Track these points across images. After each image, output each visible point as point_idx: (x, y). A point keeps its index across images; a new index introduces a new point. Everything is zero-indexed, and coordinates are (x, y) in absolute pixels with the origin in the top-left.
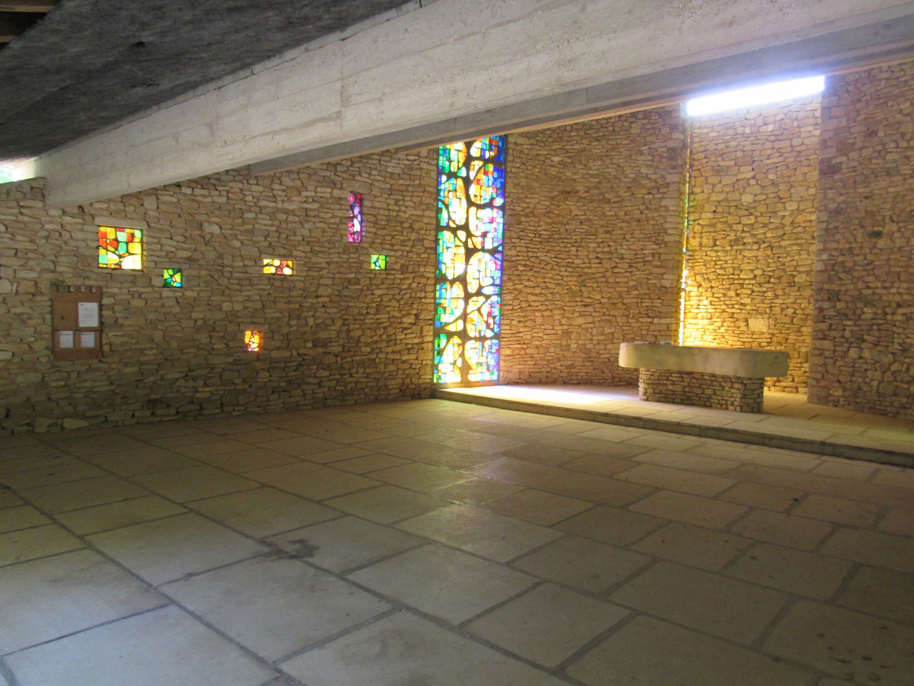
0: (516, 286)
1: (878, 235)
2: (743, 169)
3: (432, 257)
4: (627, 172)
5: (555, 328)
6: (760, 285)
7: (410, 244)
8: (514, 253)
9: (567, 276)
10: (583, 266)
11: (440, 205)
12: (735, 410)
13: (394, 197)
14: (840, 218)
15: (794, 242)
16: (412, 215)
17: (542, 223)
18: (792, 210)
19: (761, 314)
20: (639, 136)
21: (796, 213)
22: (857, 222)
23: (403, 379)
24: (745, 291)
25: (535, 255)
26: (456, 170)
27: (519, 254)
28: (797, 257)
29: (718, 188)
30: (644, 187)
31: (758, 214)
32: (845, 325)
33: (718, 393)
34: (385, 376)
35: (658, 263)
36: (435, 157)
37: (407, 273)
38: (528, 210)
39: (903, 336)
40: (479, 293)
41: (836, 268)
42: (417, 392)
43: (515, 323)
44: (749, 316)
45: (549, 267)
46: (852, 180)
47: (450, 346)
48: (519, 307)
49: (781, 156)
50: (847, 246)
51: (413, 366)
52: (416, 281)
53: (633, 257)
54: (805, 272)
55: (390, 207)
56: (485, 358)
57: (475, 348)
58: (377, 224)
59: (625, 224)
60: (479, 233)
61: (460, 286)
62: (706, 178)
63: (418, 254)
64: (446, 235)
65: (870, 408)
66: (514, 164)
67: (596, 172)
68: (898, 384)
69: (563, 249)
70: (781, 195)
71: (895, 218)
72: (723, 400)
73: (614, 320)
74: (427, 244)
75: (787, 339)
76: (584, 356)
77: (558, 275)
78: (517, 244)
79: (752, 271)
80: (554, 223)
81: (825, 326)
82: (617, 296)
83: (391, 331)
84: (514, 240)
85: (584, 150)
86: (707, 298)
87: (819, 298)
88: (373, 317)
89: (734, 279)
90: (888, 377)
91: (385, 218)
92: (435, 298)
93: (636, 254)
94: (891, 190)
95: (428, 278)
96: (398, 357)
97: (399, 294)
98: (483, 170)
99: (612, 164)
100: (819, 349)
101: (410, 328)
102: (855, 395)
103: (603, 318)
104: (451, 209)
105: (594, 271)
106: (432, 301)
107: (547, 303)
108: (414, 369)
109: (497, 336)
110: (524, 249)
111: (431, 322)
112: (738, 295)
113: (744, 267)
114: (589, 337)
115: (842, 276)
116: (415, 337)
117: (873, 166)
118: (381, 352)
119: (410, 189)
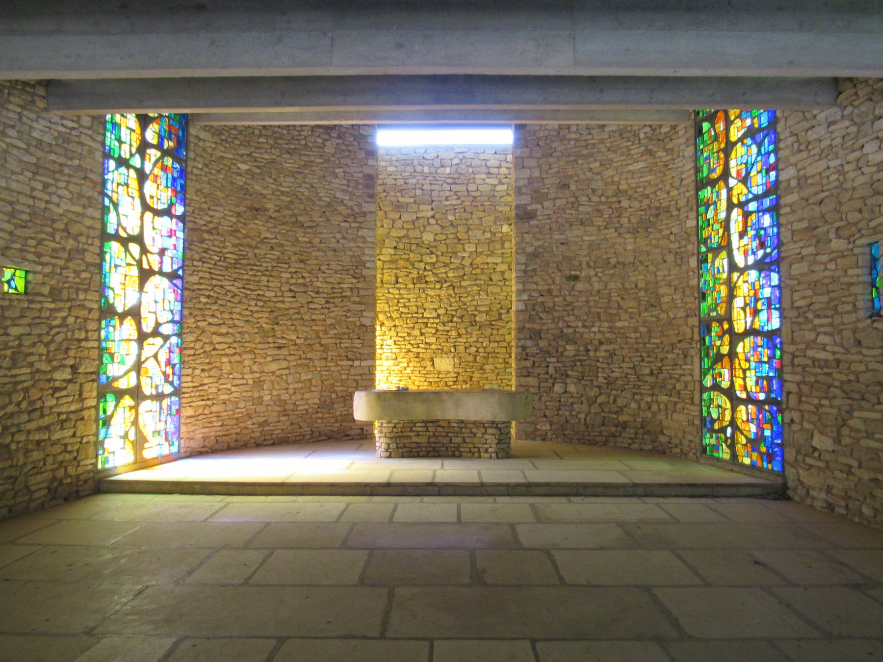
0: (199, 323)
1: (576, 278)
2: (422, 207)
3: (96, 278)
4: (321, 195)
5: (246, 376)
6: (444, 324)
7: (66, 255)
8: (195, 279)
9: (257, 312)
10: (275, 299)
11: (107, 202)
12: (491, 457)
13: (42, 179)
14: (538, 261)
15: (474, 283)
16: (67, 211)
17: (227, 244)
18: (471, 252)
19: (446, 353)
20: (333, 156)
21: (475, 254)
22: (555, 265)
23: (53, 470)
24: (430, 330)
25: (220, 283)
26: (128, 157)
27: (202, 281)
28: (477, 297)
29: (399, 224)
30: (340, 214)
31: (440, 254)
32: (549, 362)
33: (467, 440)
34: (25, 470)
35: (358, 299)
36: (101, 131)
37: (61, 300)
38: (211, 226)
39: (607, 371)
40: (156, 333)
41: (537, 308)
42: (75, 489)
43: (198, 372)
44: (434, 355)
45: (236, 300)
46: (548, 227)
47: (120, 410)
48: (202, 351)
49: (458, 199)
50: (546, 287)
51: (69, 448)
52: (73, 313)
53: (330, 291)
54: (484, 312)
55: (35, 193)
56: (163, 423)
57: (151, 411)
58: (14, 217)
59: (320, 254)
60: (155, 249)
61: (133, 322)
62: (386, 213)
63: (77, 273)
64: (114, 248)
65: (579, 440)
66: (195, 164)
67: (288, 190)
68: (606, 415)
69: (252, 278)
70: (459, 235)
71: (592, 264)
72: (474, 447)
73: (311, 364)
74: (90, 258)
75: (471, 378)
76: (279, 409)
77: (247, 309)
78: (199, 269)
79: (436, 310)
80: (241, 245)
81: (529, 364)
82: (314, 336)
83: (35, 394)
84: (195, 263)
85: (273, 162)
86: (391, 338)
87: (522, 336)
88: (7, 372)
89: (418, 318)
90: (595, 409)
91: (28, 211)
92: (99, 340)
93: (333, 288)
94: (586, 238)
95: (90, 310)
96: (46, 437)
97: (48, 334)
98: (160, 164)
99: (305, 182)
100: (524, 386)
101: (65, 388)
102: (563, 428)
103: (300, 362)
104: (121, 209)
105: (287, 306)
106: (96, 344)
107: (235, 345)
108: (70, 452)
109: (177, 392)
110: (207, 275)
111: (94, 377)
112: (422, 334)
113: (426, 305)
114: (285, 385)
115: (543, 315)
116: (72, 402)
117: (567, 216)
118: (19, 431)
119: (66, 170)
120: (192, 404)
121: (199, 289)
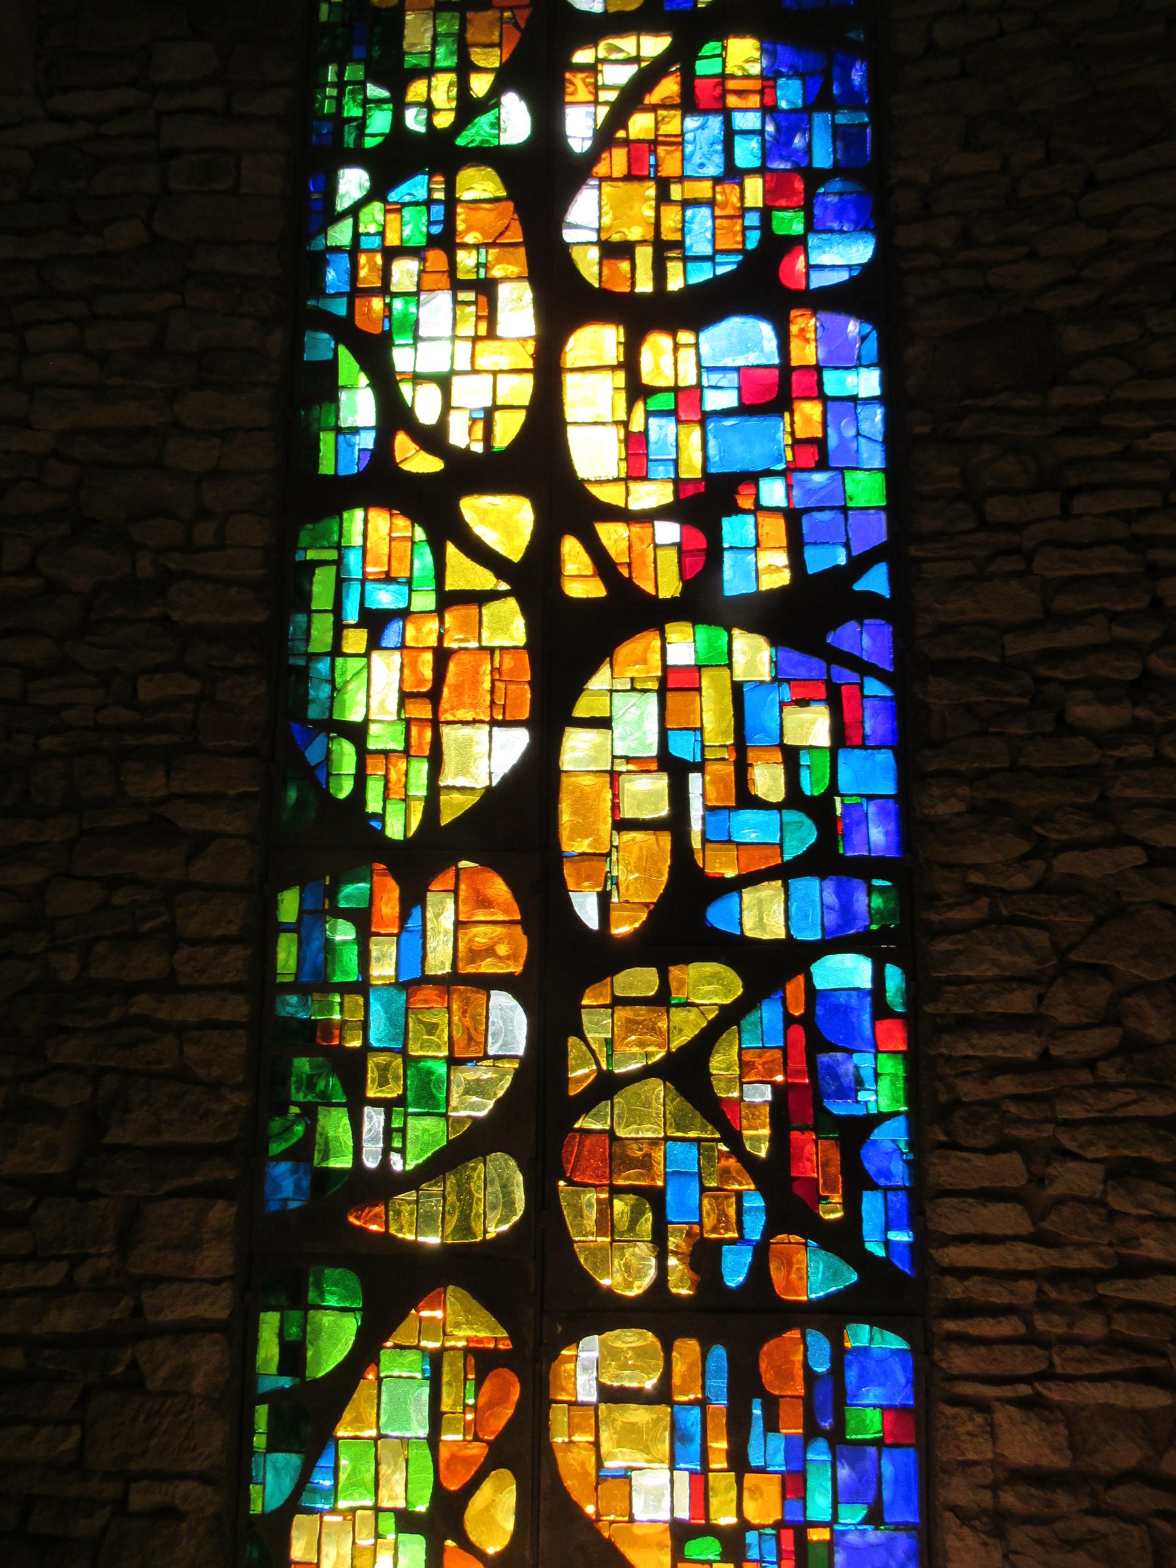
0: (1064, 863)
120: (1053, 1393)
121: (1053, 656)
